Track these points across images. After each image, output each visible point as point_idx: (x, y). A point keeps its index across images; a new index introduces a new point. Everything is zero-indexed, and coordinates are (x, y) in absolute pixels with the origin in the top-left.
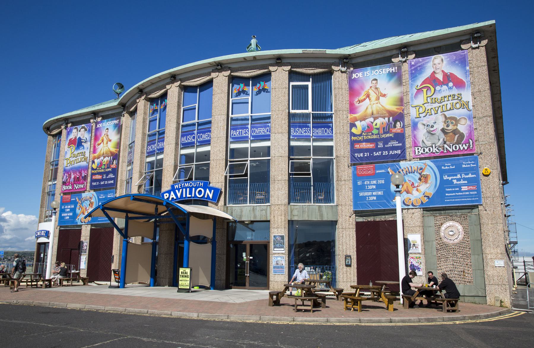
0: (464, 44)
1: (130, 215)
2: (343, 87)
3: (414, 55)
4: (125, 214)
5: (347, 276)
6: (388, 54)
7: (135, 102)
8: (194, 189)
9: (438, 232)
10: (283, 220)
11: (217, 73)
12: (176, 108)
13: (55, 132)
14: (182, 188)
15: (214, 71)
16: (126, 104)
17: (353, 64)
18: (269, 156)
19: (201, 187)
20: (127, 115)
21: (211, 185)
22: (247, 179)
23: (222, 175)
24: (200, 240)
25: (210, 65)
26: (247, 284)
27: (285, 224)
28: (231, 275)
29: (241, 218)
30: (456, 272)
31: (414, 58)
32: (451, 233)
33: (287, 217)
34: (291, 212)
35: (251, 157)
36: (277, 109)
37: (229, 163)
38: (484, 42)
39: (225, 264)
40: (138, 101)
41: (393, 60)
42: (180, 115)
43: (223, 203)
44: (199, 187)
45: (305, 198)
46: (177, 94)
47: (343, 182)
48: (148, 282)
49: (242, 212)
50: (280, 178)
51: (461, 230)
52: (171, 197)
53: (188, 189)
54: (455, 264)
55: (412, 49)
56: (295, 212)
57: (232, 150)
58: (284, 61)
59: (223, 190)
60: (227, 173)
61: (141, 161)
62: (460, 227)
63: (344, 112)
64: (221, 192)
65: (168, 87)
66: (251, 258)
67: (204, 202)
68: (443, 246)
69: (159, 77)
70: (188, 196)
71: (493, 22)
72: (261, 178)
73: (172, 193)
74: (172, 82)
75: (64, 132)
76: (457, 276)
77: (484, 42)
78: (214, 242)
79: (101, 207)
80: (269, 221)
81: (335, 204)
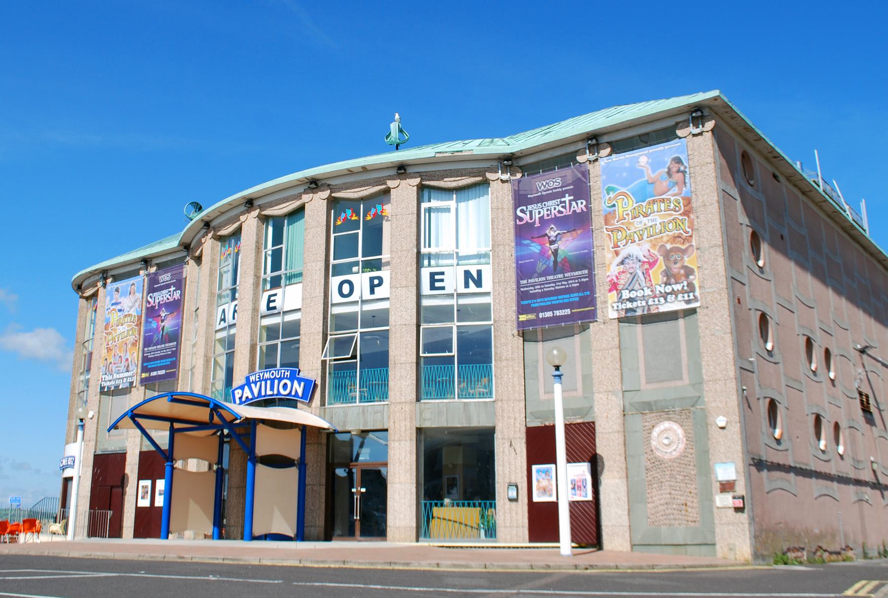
0: (681, 128)
1: (177, 425)
2: (505, 206)
3: (608, 150)
4: (168, 424)
5: (511, 517)
6: (572, 149)
7: (200, 244)
9: (648, 438)
10: (408, 428)
11: (311, 195)
12: (253, 252)
13: (88, 293)
14: (261, 381)
15: (305, 192)
16: (190, 245)
17: (520, 167)
20: (192, 262)
21: (302, 375)
22: (360, 361)
23: (318, 358)
24: (277, 461)
27: (411, 434)
29: (344, 426)
30: (674, 506)
31: (610, 155)
32: (666, 442)
33: (414, 422)
34: (421, 414)
35: (361, 328)
36: (400, 248)
37: (329, 337)
38: (710, 125)
39: (323, 500)
40: (203, 240)
41: (578, 158)
42: (260, 263)
43: (319, 403)
44: (284, 378)
45: (443, 389)
46: (254, 229)
47: (504, 363)
48: (210, 533)
49: (346, 415)
50: (403, 359)
51: (681, 436)
53: (269, 382)
54: (673, 492)
55: (606, 139)
56: (427, 415)
57: (337, 317)
58: (410, 170)
59: (319, 382)
60: (325, 356)
61: (207, 339)
62: (680, 431)
63: (507, 247)
64: (315, 386)
65: (242, 218)
66: (363, 490)
67: (290, 402)
68: (657, 463)
69: (229, 204)
70: (269, 392)
71: (715, 93)
72: (377, 360)
73: (246, 388)
74: (248, 211)
75: (102, 292)
76: (676, 512)
77: (710, 125)
78: (302, 465)
79: (130, 414)
80: (386, 430)
81: (493, 399)
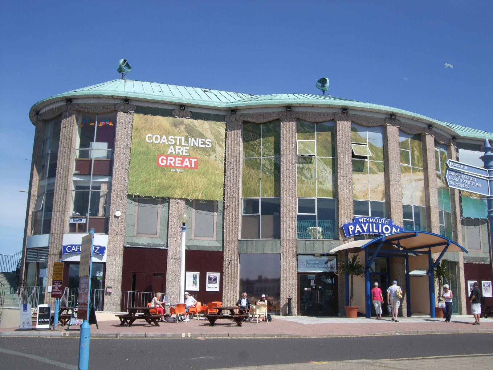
8: (380, 225)
14: (369, 223)
18: (314, 200)
19: (387, 225)
25: (117, 98)
26: (281, 315)
28: (101, 293)
44: (385, 224)
52: (357, 230)
73: (358, 226)
